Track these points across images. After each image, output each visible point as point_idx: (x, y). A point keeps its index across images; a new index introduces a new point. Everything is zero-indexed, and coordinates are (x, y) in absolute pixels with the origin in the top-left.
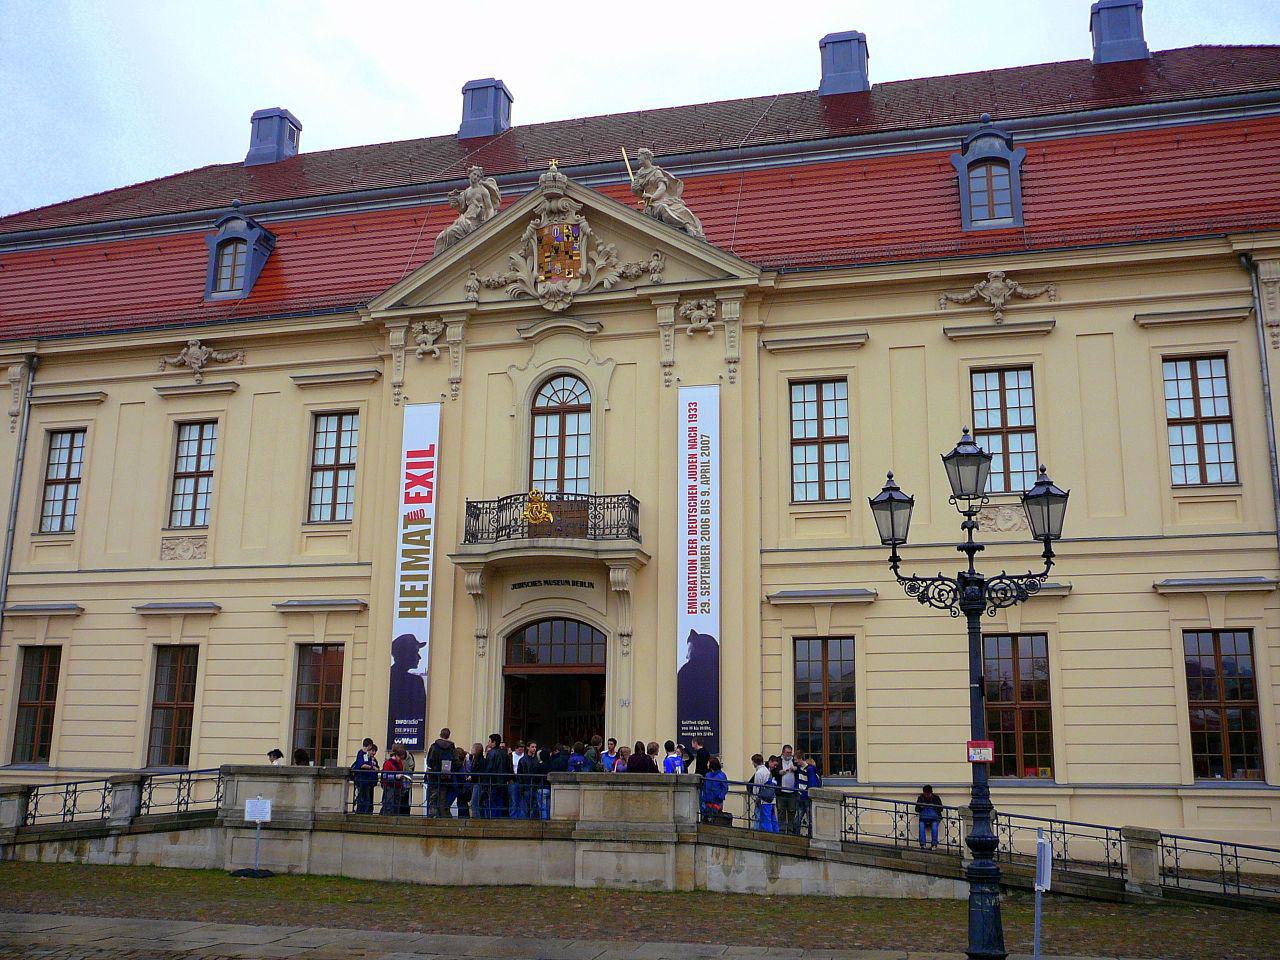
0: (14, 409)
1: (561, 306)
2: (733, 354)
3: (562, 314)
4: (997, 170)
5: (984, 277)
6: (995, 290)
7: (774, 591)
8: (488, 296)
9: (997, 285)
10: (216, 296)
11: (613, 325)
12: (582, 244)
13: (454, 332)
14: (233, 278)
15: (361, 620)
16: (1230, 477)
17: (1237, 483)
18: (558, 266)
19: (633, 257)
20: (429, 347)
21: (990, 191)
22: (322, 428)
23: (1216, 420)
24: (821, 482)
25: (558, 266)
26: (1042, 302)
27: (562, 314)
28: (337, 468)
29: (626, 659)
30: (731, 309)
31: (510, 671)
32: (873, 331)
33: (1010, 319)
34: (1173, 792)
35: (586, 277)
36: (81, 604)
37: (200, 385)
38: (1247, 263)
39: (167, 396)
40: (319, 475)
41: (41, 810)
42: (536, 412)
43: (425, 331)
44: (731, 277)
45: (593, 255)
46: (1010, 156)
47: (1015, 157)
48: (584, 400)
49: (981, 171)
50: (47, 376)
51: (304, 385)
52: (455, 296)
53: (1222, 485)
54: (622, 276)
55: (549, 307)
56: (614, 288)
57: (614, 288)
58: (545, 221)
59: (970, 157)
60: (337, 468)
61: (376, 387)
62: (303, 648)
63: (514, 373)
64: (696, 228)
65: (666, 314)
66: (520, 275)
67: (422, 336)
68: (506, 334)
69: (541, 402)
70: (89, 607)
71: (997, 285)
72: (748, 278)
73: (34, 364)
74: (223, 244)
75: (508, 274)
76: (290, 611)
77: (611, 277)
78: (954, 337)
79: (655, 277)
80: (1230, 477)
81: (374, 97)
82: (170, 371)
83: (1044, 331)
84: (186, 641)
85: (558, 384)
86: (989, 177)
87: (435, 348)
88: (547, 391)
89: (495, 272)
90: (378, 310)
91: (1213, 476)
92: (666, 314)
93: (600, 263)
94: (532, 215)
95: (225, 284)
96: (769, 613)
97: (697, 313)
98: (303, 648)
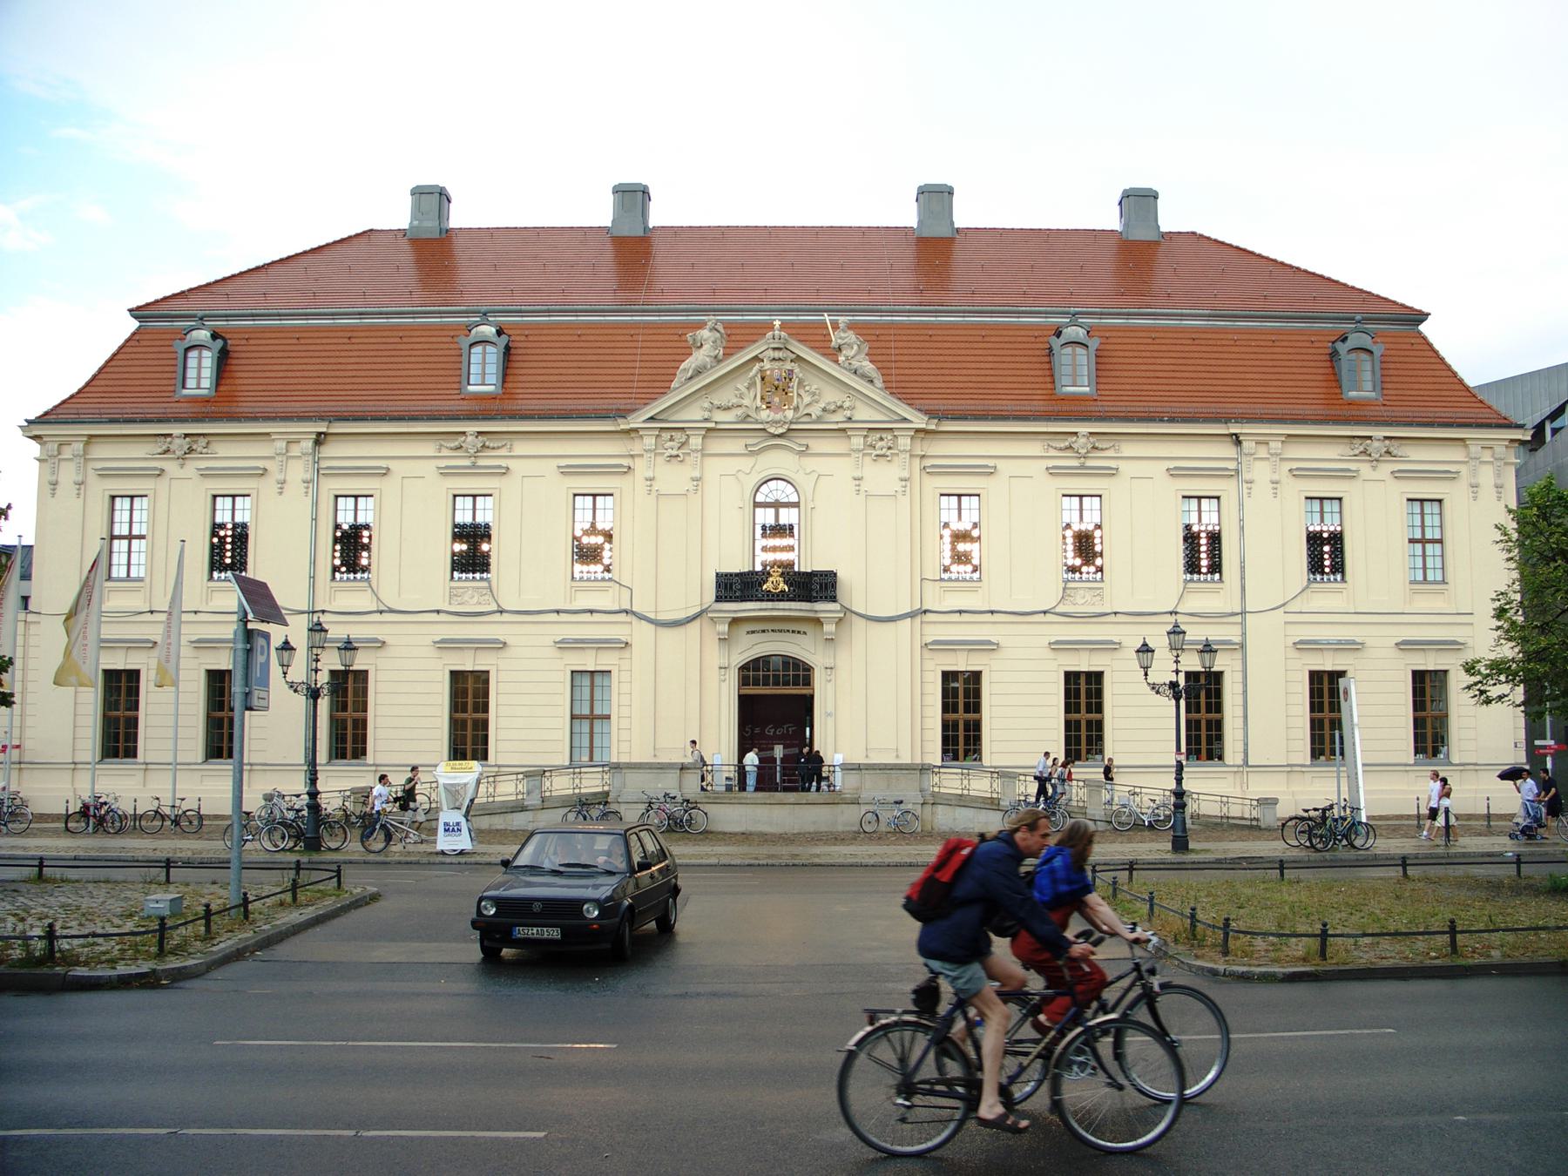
0: (308, 476)
1: (781, 431)
2: (906, 474)
3: (779, 436)
4: (1080, 350)
5: (1370, 438)
6: (179, 445)
7: (929, 640)
8: (720, 416)
9: (1082, 440)
10: (185, 392)
11: (818, 445)
12: (795, 382)
13: (696, 442)
14: (199, 378)
15: (626, 654)
16: (1439, 578)
17: (1444, 582)
18: (777, 399)
19: (831, 396)
20: (675, 452)
21: (1074, 365)
22: (219, 506)
23: (121, 537)
24: (1425, 568)
25: (777, 399)
26: (503, 452)
27: (779, 436)
28: (130, 537)
29: (829, 685)
30: (904, 442)
31: (751, 690)
32: (1000, 464)
33: (1090, 463)
34: (1291, 768)
35: (796, 409)
36: (386, 638)
37: (474, 466)
38: (1237, 440)
39: (446, 473)
40: (116, 542)
41: (555, 786)
42: (757, 505)
43: (672, 439)
44: (905, 420)
45: (802, 392)
46: (1374, 349)
47: (1094, 344)
48: (794, 498)
49: (1068, 350)
50: (329, 450)
51: (566, 472)
52: (694, 413)
53: (1435, 582)
54: (824, 410)
55: (772, 430)
56: (819, 420)
57: (819, 420)
58: (767, 365)
59: (1062, 340)
60: (130, 537)
61: (628, 478)
62: (456, 676)
63: (740, 475)
64: (879, 383)
65: (857, 442)
66: (746, 402)
67: (670, 444)
68: (735, 445)
69: (760, 498)
70: (1369, 642)
71: (1082, 440)
72: (920, 421)
73: (320, 439)
74: (187, 350)
75: (735, 401)
76: (1405, 646)
77: (815, 411)
78: (1053, 472)
79: (848, 413)
80: (1439, 578)
81: (531, 182)
82: (445, 452)
83: (1112, 473)
84: (129, 667)
85: (772, 484)
86: (484, 353)
87: (680, 452)
88: (764, 489)
89: (725, 396)
90: (636, 421)
91: (1430, 577)
92: (857, 442)
93: (807, 399)
94: (756, 359)
95: (191, 383)
96: (927, 655)
97: (880, 444)
98: (456, 676)
